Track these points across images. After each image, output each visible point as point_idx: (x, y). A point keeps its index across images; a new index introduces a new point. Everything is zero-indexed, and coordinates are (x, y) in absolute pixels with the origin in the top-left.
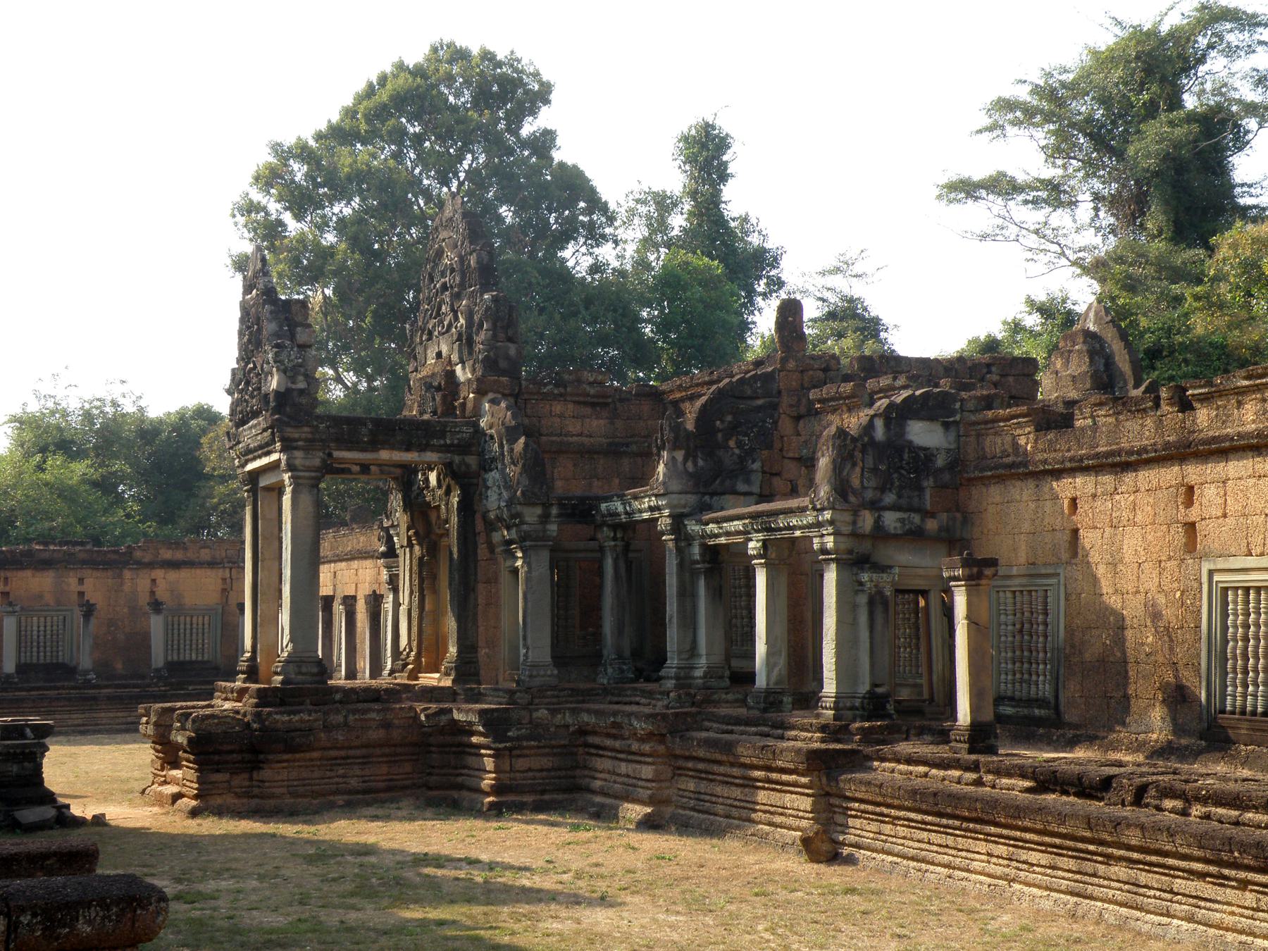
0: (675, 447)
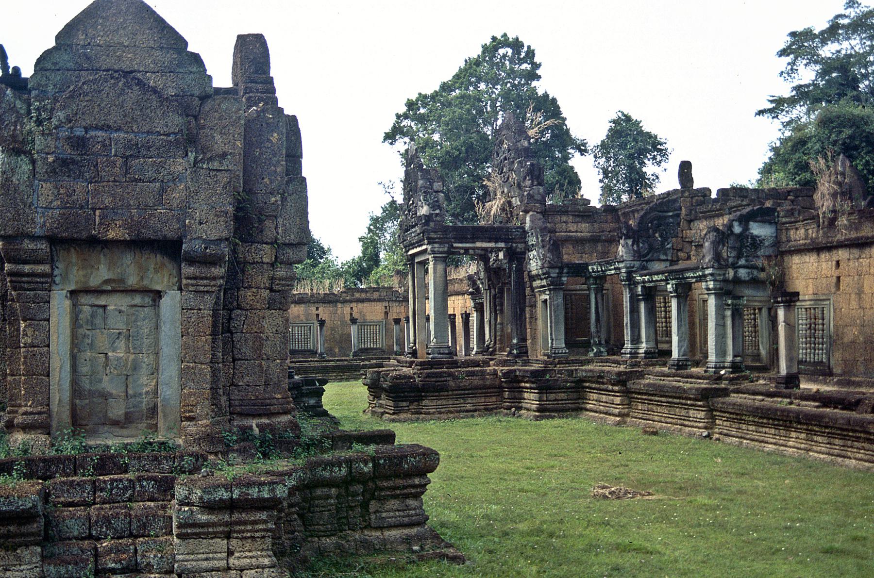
0: (627, 237)
